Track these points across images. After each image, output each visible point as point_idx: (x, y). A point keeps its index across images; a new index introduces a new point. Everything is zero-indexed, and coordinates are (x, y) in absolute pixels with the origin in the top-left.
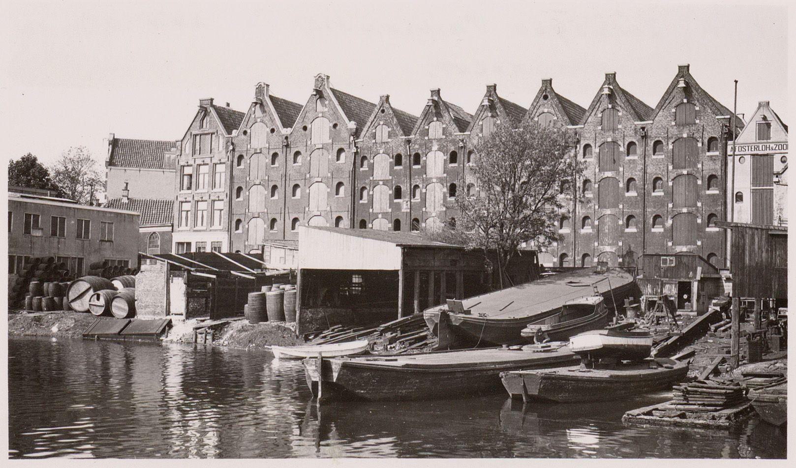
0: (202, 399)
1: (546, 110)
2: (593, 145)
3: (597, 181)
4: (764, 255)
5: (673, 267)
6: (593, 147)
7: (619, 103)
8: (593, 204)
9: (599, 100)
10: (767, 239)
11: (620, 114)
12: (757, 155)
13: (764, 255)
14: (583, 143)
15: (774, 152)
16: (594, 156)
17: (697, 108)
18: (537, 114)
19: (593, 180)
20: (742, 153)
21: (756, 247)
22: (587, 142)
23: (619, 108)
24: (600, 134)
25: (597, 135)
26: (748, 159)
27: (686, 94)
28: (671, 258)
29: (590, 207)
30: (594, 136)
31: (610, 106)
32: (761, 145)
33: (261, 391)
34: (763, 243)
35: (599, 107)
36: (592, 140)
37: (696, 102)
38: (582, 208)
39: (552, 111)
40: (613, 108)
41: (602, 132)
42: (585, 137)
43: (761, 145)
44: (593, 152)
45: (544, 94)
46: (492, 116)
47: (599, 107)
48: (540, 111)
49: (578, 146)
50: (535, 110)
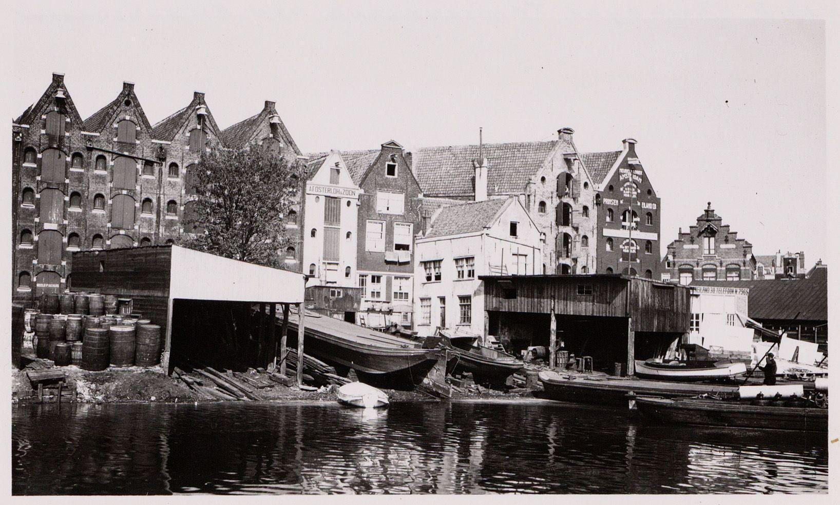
0: (490, 476)
1: (128, 118)
2: (179, 165)
3: (183, 203)
4: (650, 300)
5: (341, 299)
6: (180, 167)
7: (208, 125)
8: (178, 227)
9: (188, 118)
10: (651, 289)
11: (281, 145)
12: (329, 197)
13: (650, 300)
14: (169, 161)
15: (342, 196)
16: (180, 176)
17: (139, 128)
18: (117, 120)
19: (178, 202)
20: (318, 193)
21: (645, 295)
22: (174, 161)
23: (208, 131)
24: (187, 154)
25: (185, 154)
26: (323, 199)
27: (272, 129)
28: (339, 290)
29: (175, 230)
30: (180, 154)
31: (199, 127)
32: (333, 188)
33: (325, 465)
34: (649, 291)
35: (187, 125)
36: (179, 160)
37: (281, 139)
38: (165, 231)
39: (135, 120)
40: (203, 129)
41: (190, 153)
42: (171, 155)
43: (333, 188)
44: (179, 173)
45: (126, 99)
46: (60, 112)
47: (187, 125)
48: (121, 116)
49: (164, 163)
50: (115, 115)
